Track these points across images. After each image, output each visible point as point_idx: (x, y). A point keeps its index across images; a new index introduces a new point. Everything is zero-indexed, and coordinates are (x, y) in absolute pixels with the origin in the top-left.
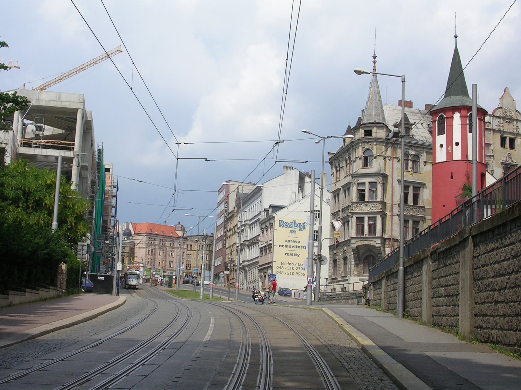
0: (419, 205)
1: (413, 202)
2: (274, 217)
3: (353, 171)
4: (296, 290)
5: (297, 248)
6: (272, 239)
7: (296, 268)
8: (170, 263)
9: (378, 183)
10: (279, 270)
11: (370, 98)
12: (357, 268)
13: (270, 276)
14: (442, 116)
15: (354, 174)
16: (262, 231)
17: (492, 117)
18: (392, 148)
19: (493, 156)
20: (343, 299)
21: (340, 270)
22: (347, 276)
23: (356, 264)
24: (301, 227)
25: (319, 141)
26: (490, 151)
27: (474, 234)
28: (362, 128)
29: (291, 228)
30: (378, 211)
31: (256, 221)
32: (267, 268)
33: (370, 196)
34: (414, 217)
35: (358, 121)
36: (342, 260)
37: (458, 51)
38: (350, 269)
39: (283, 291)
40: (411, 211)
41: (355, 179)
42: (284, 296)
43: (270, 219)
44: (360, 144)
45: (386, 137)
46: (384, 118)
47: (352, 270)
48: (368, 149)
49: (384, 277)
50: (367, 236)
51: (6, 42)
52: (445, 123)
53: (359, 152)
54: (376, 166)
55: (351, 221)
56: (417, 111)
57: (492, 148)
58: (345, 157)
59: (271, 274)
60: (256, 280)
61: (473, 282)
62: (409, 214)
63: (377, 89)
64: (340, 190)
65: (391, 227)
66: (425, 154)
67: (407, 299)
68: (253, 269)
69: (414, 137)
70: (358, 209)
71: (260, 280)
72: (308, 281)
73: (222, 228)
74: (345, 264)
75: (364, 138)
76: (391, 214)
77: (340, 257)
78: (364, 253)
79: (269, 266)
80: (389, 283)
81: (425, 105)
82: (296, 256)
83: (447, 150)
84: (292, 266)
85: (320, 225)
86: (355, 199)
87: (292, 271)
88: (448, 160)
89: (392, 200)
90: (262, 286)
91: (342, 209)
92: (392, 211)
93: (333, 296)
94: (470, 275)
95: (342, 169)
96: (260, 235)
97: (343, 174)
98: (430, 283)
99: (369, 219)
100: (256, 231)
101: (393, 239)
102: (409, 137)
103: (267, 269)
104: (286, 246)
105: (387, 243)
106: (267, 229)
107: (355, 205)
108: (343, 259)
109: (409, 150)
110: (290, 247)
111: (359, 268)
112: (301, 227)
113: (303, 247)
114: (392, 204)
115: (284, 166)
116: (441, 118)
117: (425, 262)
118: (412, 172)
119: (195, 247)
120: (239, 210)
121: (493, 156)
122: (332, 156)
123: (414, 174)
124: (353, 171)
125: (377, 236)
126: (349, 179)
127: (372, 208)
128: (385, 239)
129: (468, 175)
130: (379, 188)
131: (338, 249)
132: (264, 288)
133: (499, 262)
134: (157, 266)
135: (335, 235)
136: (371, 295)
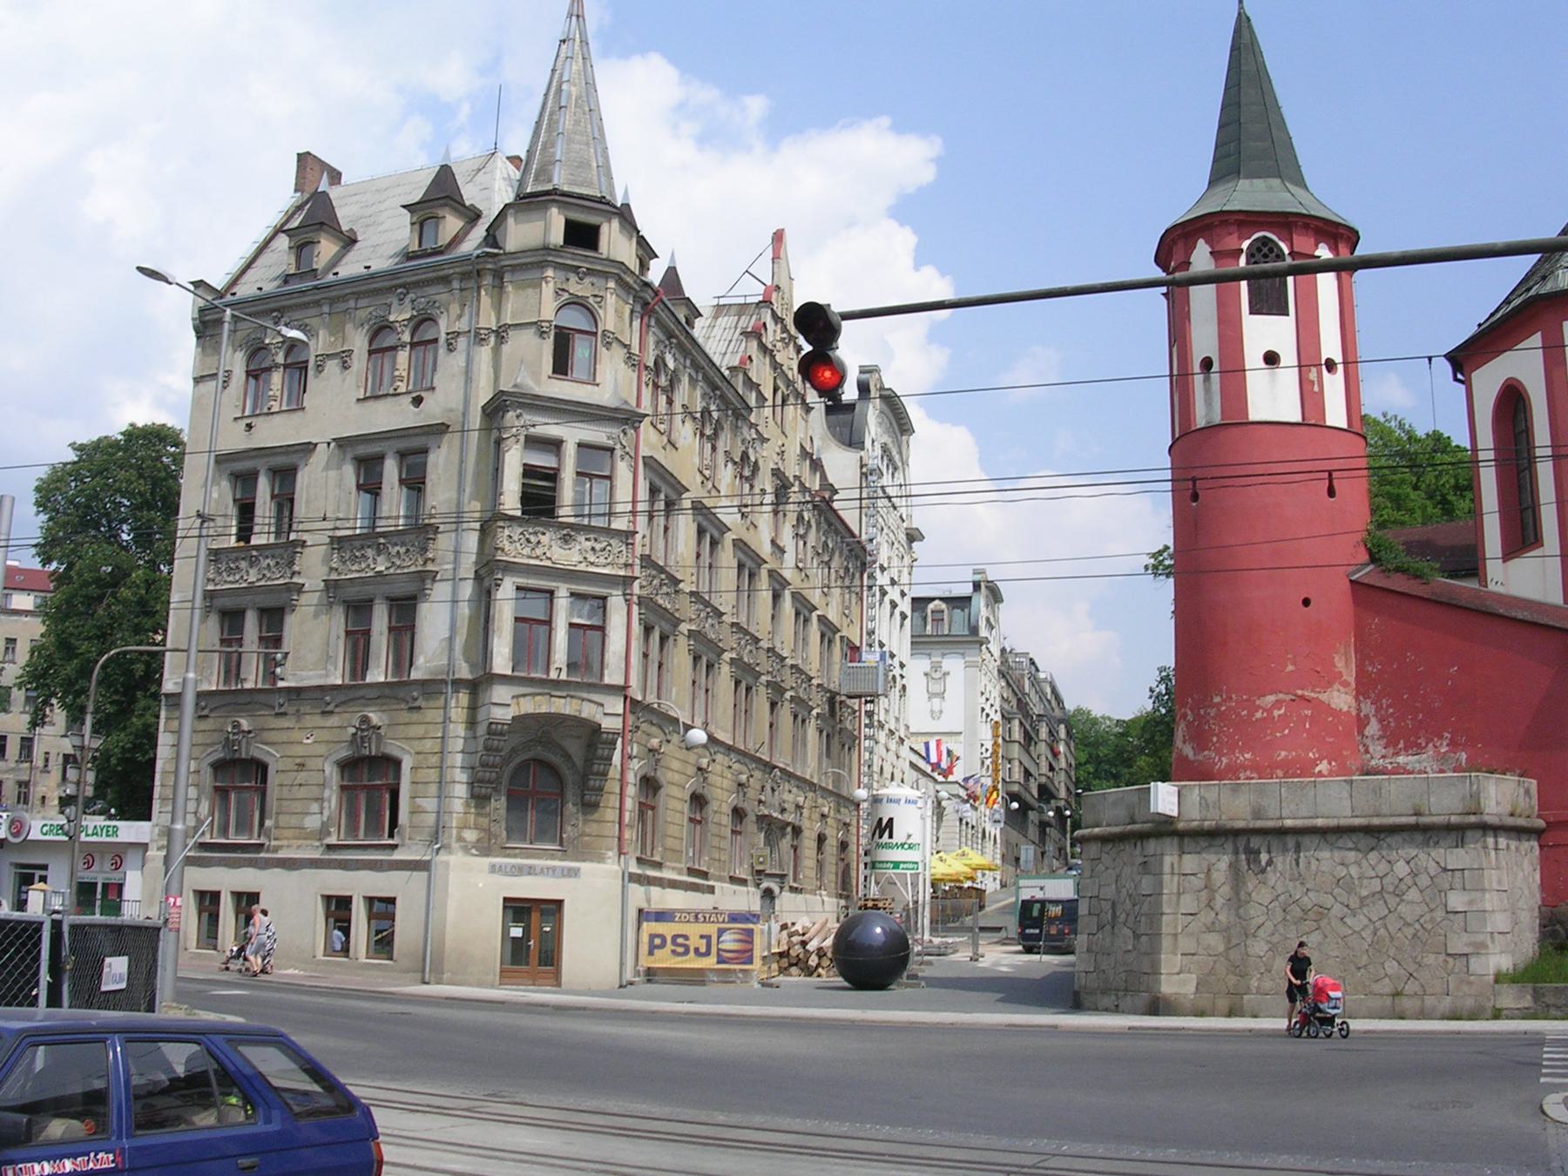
9: (618, 453)
12: (478, 814)
28: (563, 206)
30: (613, 572)
44: (550, 273)
50: (563, 676)
70: (527, 551)
78: (514, 751)
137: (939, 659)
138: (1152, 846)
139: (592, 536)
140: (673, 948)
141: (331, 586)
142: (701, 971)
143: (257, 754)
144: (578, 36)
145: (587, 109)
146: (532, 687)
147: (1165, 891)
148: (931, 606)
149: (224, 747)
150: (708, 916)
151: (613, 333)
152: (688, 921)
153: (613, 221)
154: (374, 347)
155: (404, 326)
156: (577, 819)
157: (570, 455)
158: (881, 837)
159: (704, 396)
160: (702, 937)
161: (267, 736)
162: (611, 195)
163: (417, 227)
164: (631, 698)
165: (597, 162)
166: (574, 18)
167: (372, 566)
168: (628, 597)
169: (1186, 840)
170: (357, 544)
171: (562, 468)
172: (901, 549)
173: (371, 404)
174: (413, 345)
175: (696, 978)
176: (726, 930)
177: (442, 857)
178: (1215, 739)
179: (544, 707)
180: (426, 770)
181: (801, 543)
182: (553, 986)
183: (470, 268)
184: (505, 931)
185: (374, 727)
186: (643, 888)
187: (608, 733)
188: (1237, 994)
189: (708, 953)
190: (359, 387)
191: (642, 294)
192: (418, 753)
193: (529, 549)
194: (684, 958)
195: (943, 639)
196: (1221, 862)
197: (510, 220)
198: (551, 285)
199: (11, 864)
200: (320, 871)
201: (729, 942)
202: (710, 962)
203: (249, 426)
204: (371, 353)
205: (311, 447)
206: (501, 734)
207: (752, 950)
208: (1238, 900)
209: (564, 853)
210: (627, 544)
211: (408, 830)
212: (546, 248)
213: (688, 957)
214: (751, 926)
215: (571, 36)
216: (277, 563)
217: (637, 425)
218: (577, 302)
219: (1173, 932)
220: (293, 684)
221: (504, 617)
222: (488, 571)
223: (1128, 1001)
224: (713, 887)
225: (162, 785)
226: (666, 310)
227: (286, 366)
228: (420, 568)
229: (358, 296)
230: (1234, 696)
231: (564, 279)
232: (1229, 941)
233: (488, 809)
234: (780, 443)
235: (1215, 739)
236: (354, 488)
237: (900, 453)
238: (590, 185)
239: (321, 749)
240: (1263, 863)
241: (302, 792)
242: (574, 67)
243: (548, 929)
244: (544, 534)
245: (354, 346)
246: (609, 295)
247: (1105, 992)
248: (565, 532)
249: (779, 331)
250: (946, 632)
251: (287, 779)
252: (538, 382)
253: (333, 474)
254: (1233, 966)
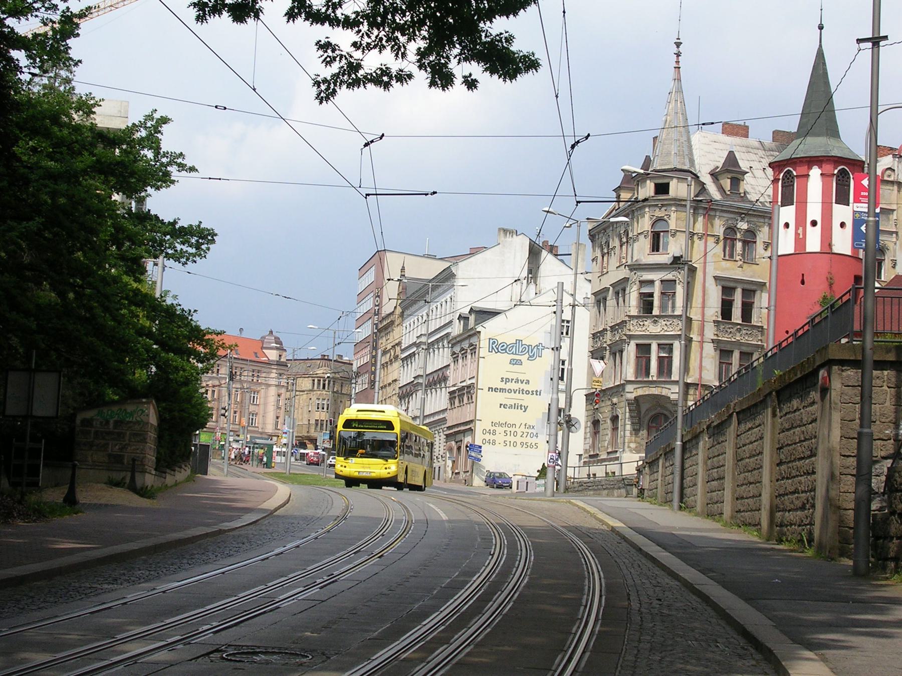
0: (752, 323)
1: (742, 317)
2: (479, 332)
3: (632, 258)
4: (521, 477)
5: (523, 393)
6: (475, 374)
7: (520, 434)
8: (251, 417)
9: (677, 282)
10: (488, 437)
11: (668, 122)
12: (636, 437)
13: (470, 449)
14: (789, 172)
15: (634, 265)
16: (454, 358)
17: (897, 159)
18: (704, 218)
19: (897, 233)
20: (604, 489)
21: (605, 441)
22: (617, 451)
23: (634, 430)
24: (533, 352)
25: (571, 225)
26: (891, 223)
27: (737, 411)
28: (651, 179)
29: (513, 353)
31: (442, 339)
32: (464, 431)
33: (663, 307)
34: (743, 346)
35: (645, 161)
36: (609, 421)
37: (823, 54)
38: (622, 439)
39: (494, 478)
40: (738, 334)
41: (635, 273)
42: (497, 488)
43: (470, 336)
44: (647, 210)
45: (695, 197)
46: (692, 161)
47: (626, 441)
48: (660, 219)
49: (661, 455)
50: (655, 379)
51: (196, 168)
52: (793, 185)
53: (645, 224)
54: (674, 247)
55: (626, 350)
56: (757, 144)
57: (895, 217)
58: (618, 229)
59: (470, 445)
60: (440, 457)
61: (736, 461)
62: (733, 340)
63: (681, 105)
64: (609, 290)
65: (699, 362)
66: (768, 228)
67: (685, 486)
68: (439, 433)
69: (748, 195)
70: (640, 329)
71: (448, 455)
72: (549, 458)
73: (368, 349)
74: (615, 429)
75: (655, 198)
76: (699, 339)
77: (605, 415)
79: (467, 428)
80: (667, 464)
81: (774, 132)
82: (521, 409)
83: (797, 234)
84: (513, 429)
85: (570, 367)
86: (634, 312)
87: (512, 439)
88: (798, 252)
89: (703, 315)
90: (452, 468)
91: (611, 327)
92: (702, 333)
93: (588, 485)
94: (733, 455)
95: (613, 252)
96: (449, 365)
97: (614, 261)
98: (705, 463)
99: (659, 347)
100: (440, 358)
101: (703, 386)
102: (738, 195)
103: (463, 434)
104: (502, 390)
105: (691, 391)
106: (464, 356)
107: (634, 322)
108: (611, 419)
109: (737, 220)
110: (510, 391)
111: (639, 437)
112: (533, 352)
113: (535, 393)
114: (703, 321)
115: (500, 229)
116: (788, 176)
117: (701, 438)
118: (741, 263)
119: (306, 384)
120: (405, 314)
121: (897, 232)
122: (596, 224)
123: (745, 266)
124: (632, 258)
125: (673, 379)
126: (624, 273)
128: (687, 386)
129: (831, 279)
130: (680, 290)
131: (603, 401)
132: (457, 471)
133: (752, 443)
134: (224, 424)
135: (594, 383)
136: (645, 482)
139: (665, 319)
166: (676, 81)
242: (670, 106)
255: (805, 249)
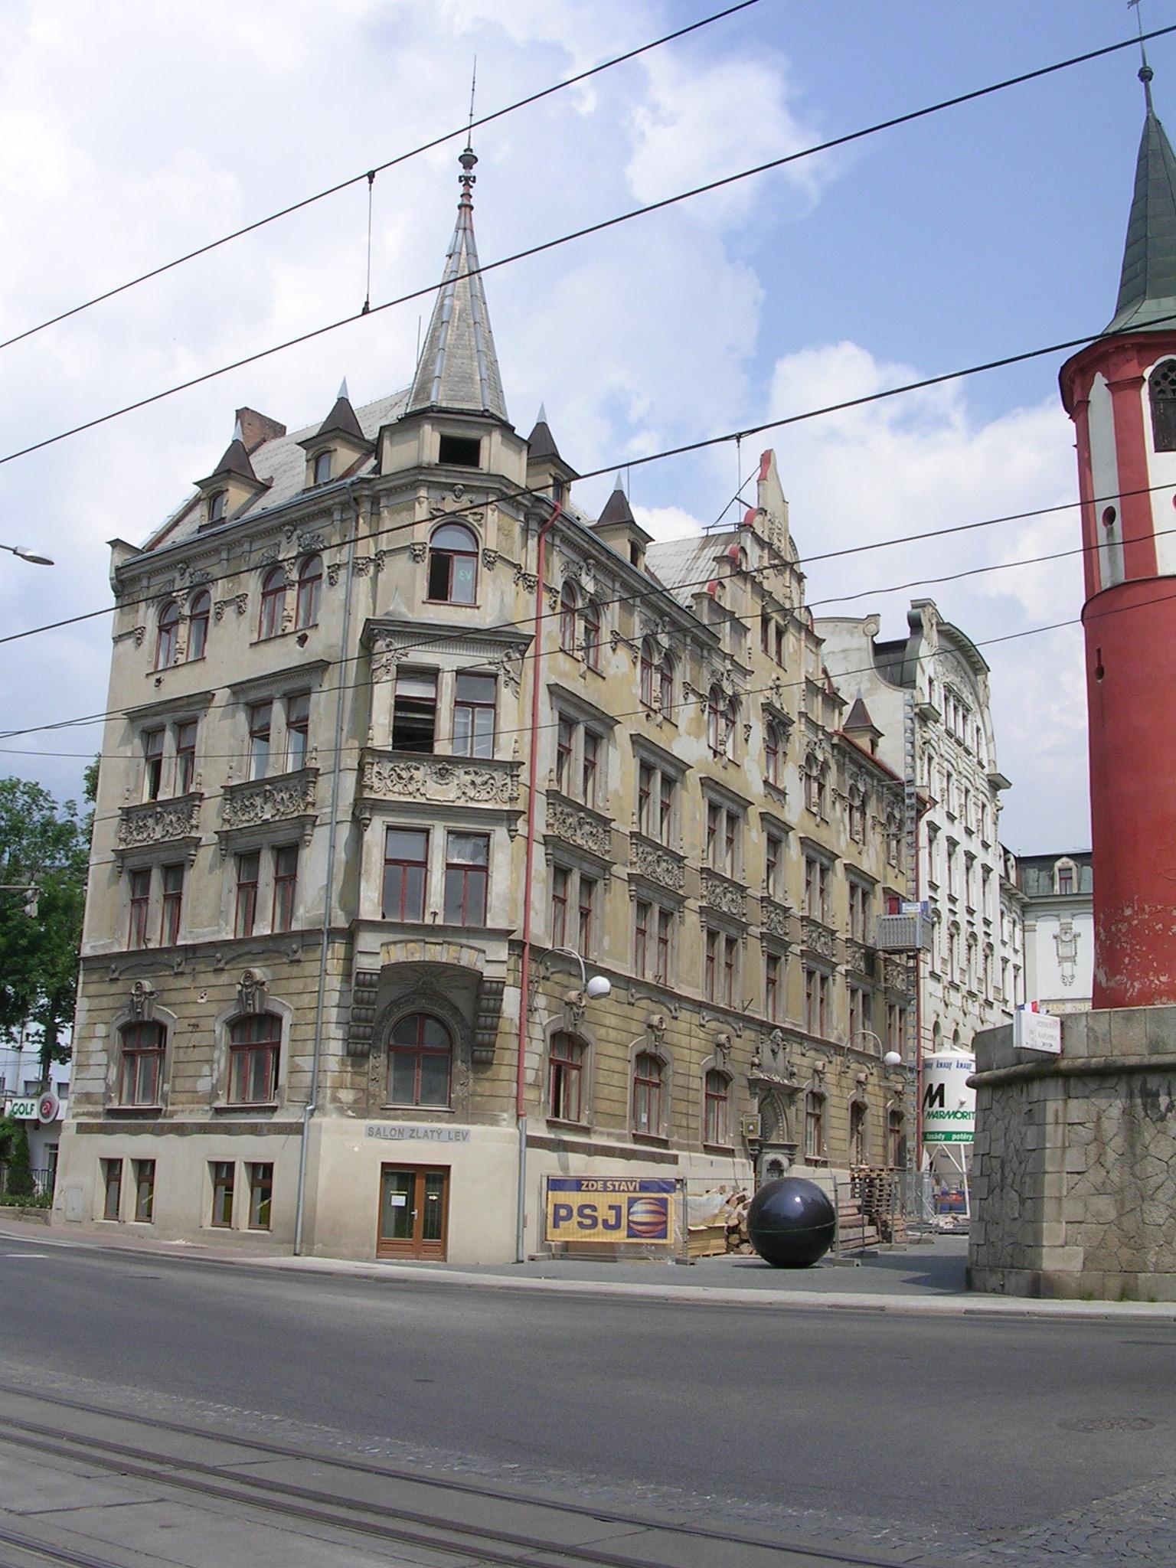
9: (502, 679)
12: (354, 1073)
28: (436, 422)
30: (497, 807)
44: (423, 493)
50: (439, 921)
70: (399, 788)
78: (394, 1003)
127: (472, 793)
137: (1069, 920)
138: (1036, 1090)
140: (580, 1219)
141: (224, 837)
142: (611, 1245)
143: (158, 1016)
144: (464, 249)
145: (472, 322)
146: (404, 933)
147: (1048, 1145)
148: (1058, 864)
149: (130, 1010)
150: (617, 1184)
151: (496, 552)
152: (596, 1190)
153: (493, 433)
154: (270, 588)
155: (291, 564)
156: (467, 1078)
157: (447, 684)
158: (931, 1106)
159: (645, 623)
160: (611, 1207)
161: (171, 997)
162: (499, 408)
163: (313, 463)
164: (532, 947)
165: (481, 374)
166: (461, 232)
167: (260, 815)
168: (513, 833)
169: (1072, 1081)
170: (247, 793)
171: (439, 698)
172: (981, 796)
173: (262, 647)
174: (302, 583)
175: (606, 1253)
176: (636, 1200)
177: (316, 1120)
178: (1126, 960)
179: (418, 955)
180: (304, 1027)
181: (815, 786)
182: (439, 1260)
183: (346, 496)
184: (385, 1199)
185: (257, 983)
186: (555, 1155)
187: (491, 982)
188: (1129, 1271)
189: (617, 1226)
190: (252, 630)
191: (537, 511)
192: (297, 1009)
193: (401, 786)
194: (592, 1231)
195: (1069, 899)
196: (1113, 1107)
197: (386, 443)
198: (425, 505)
199: (46, 1145)
200: (206, 1136)
201: (641, 1213)
202: (620, 1236)
203: (159, 681)
204: (264, 595)
205: (209, 696)
206: (372, 985)
207: (665, 1222)
208: (1133, 1154)
209: (452, 1115)
210: (512, 776)
211: (287, 1090)
212: (419, 468)
213: (596, 1230)
214: (665, 1195)
215: (457, 250)
216: (179, 818)
217: (522, 647)
218: (454, 521)
219: (1057, 1195)
220: (190, 942)
221: (373, 859)
222: (363, 810)
223: (1012, 1281)
224: (676, 1157)
225: (79, 1052)
226: (572, 528)
227: (192, 618)
228: (301, 813)
229: (252, 538)
230: (1146, 906)
231: (439, 498)
232: (1123, 1205)
233: (366, 1066)
234: (774, 676)
235: (1126, 960)
236: (247, 736)
237: (976, 694)
238: (472, 398)
239: (212, 1009)
240: (1163, 1108)
241: (195, 1055)
243: (435, 1198)
244: (417, 769)
245: (248, 590)
246: (490, 512)
247: (993, 1269)
248: (440, 766)
249: (766, 556)
250: (1075, 891)
251: (183, 1041)
252: (411, 609)
253: (228, 723)
254: (1126, 1237)
255: (1154, 567)
